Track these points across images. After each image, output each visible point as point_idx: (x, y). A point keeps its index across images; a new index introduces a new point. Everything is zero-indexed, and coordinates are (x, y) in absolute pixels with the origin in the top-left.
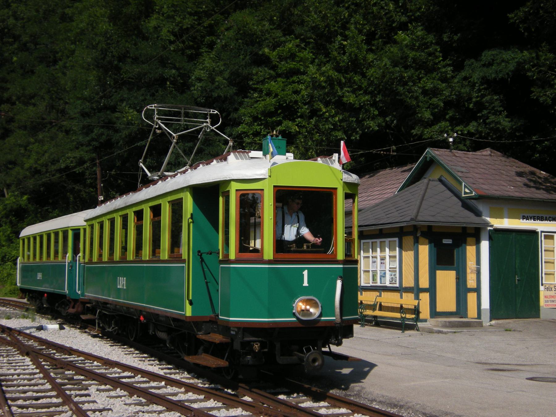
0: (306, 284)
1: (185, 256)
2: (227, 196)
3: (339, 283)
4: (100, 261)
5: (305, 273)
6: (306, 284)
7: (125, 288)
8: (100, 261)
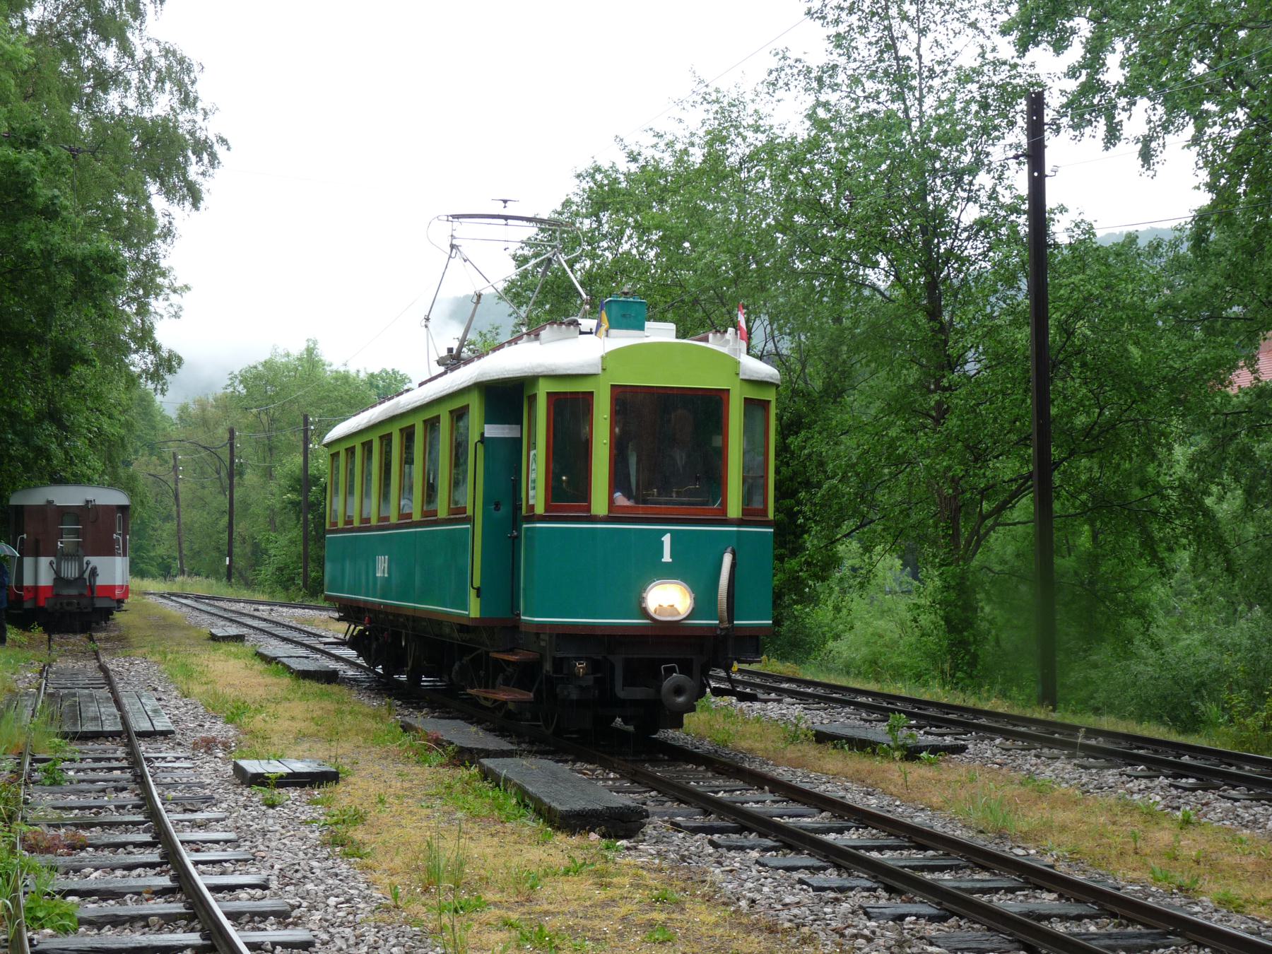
0: (667, 558)
3: (727, 559)
5: (667, 539)
6: (667, 558)
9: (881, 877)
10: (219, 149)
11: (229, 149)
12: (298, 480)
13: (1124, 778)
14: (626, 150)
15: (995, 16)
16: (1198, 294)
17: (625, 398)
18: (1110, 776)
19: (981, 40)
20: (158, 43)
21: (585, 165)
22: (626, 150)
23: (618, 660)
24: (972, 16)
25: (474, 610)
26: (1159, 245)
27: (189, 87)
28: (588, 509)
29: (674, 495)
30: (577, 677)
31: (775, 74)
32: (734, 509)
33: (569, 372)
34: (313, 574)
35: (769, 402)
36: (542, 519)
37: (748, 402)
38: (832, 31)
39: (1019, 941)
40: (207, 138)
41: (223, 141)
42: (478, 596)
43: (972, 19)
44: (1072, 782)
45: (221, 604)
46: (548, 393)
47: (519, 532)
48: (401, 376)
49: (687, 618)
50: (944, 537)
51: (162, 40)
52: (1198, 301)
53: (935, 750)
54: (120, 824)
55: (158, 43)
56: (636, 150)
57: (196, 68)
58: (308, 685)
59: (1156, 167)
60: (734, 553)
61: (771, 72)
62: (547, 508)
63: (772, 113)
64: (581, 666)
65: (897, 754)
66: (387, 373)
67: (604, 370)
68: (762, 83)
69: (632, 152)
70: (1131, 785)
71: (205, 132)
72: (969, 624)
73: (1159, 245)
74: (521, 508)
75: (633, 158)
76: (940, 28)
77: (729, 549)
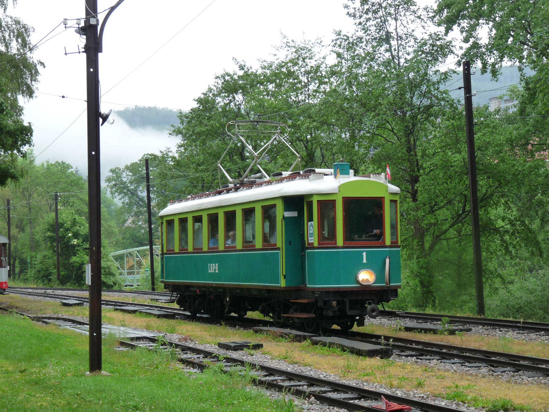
0: (365, 261)
1: (279, 245)
2: (310, 204)
3: (387, 261)
4: (183, 250)
5: (364, 254)
6: (365, 261)
7: (217, 272)
8: (183, 250)
9: (488, 363)
10: (39, 68)
11: (44, 67)
12: (52, 226)
13: (539, 336)
14: (238, 64)
15: (429, 13)
16: (521, 134)
17: (349, 202)
18: (533, 336)
19: (423, 23)
20: (11, 18)
21: (220, 73)
22: (238, 64)
23: (347, 301)
24: (418, 14)
25: (283, 283)
26: (499, 110)
27: (27, 39)
28: (336, 244)
29: (364, 237)
30: (333, 307)
31: (335, 42)
32: (388, 242)
33: (326, 192)
34: (62, 273)
35: (397, 201)
37: (391, 201)
38: (358, 21)
39: (547, 375)
40: (33, 62)
41: (42, 64)
42: (285, 278)
43: (419, 14)
44: (519, 339)
45: (17, 289)
46: (318, 201)
47: (305, 253)
48: (67, 165)
49: (373, 283)
50: (417, 246)
51: (14, 16)
52: (521, 137)
53: (461, 330)
54: (417, 329)
55: (11, 18)
56: (243, 63)
57: (31, 30)
59: (498, 76)
60: (389, 258)
61: (333, 41)
62: (319, 244)
63: (320, 52)
64: (334, 303)
65: (446, 333)
66: (59, 164)
67: (339, 191)
68: (329, 45)
69: (241, 65)
70: (542, 338)
71: (32, 59)
72: (430, 283)
73: (499, 110)
74: (305, 244)
75: (241, 68)
76: (403, 18)
77: (388, 257)
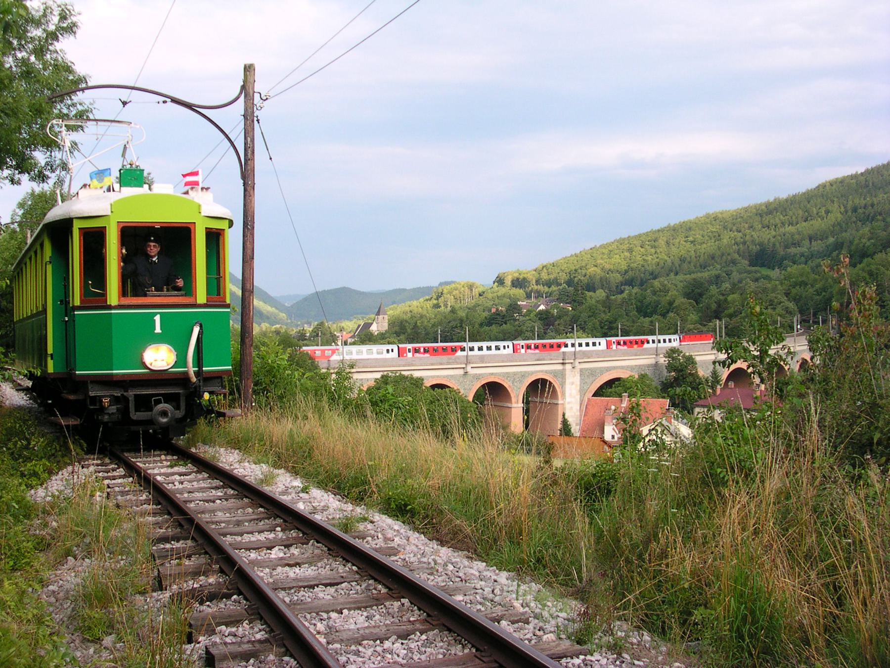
0: (158, 330)
3: (196, 330)
5: (157, 318)
6: (158, 330)
32: (201, 297)
36: (116, 307)
42: (52, 359)
58: (534, 415)
74: (69, 303)
